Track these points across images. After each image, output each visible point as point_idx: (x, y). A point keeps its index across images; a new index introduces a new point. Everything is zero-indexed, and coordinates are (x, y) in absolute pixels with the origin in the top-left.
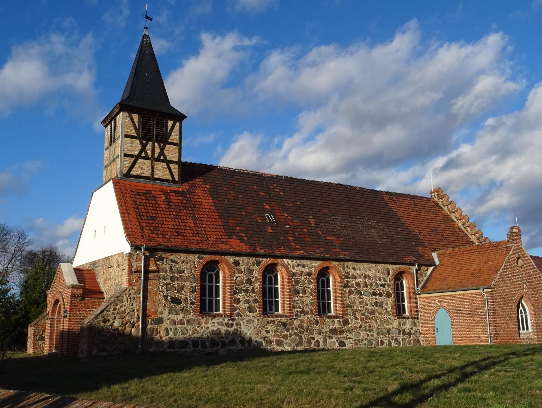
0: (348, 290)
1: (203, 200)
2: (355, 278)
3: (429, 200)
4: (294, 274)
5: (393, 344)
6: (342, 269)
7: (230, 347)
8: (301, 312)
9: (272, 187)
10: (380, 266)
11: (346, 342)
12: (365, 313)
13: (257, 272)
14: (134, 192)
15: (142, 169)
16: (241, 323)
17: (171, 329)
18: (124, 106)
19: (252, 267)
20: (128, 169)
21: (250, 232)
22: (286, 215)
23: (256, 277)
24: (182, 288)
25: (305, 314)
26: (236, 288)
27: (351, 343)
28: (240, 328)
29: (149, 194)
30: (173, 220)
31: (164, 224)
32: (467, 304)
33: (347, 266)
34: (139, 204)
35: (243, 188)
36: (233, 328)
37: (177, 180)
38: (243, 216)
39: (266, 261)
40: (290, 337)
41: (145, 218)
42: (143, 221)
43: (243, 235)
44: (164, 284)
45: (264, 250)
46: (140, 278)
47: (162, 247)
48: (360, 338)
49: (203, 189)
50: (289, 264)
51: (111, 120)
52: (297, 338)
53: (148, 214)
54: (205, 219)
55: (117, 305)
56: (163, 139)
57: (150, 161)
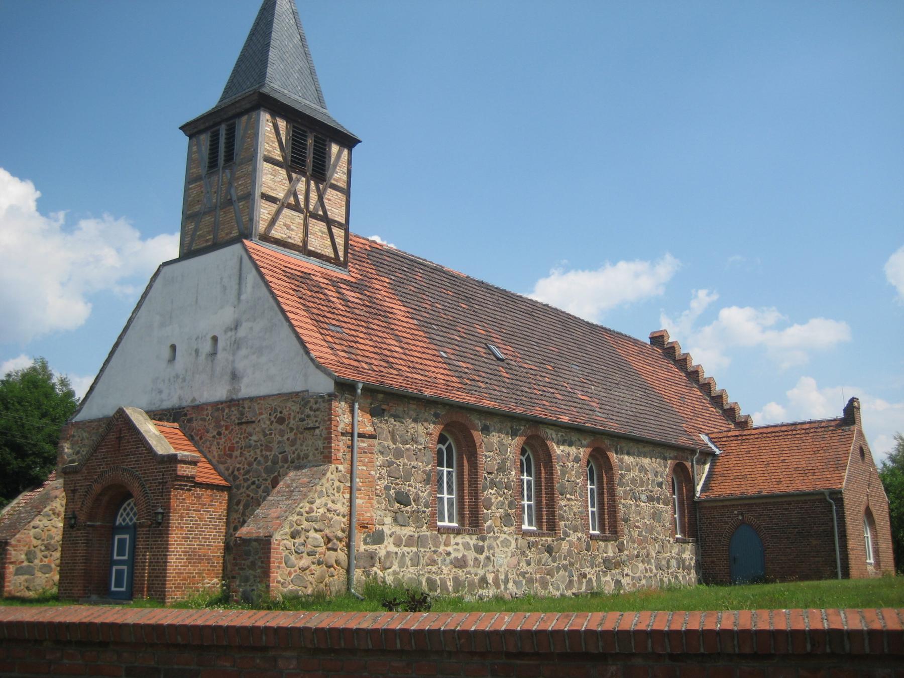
7: (480, 592)
15: (288, 227)
16: (494, 544)
17: (396, 553)
56: (320, 173)
57: (302, 216)
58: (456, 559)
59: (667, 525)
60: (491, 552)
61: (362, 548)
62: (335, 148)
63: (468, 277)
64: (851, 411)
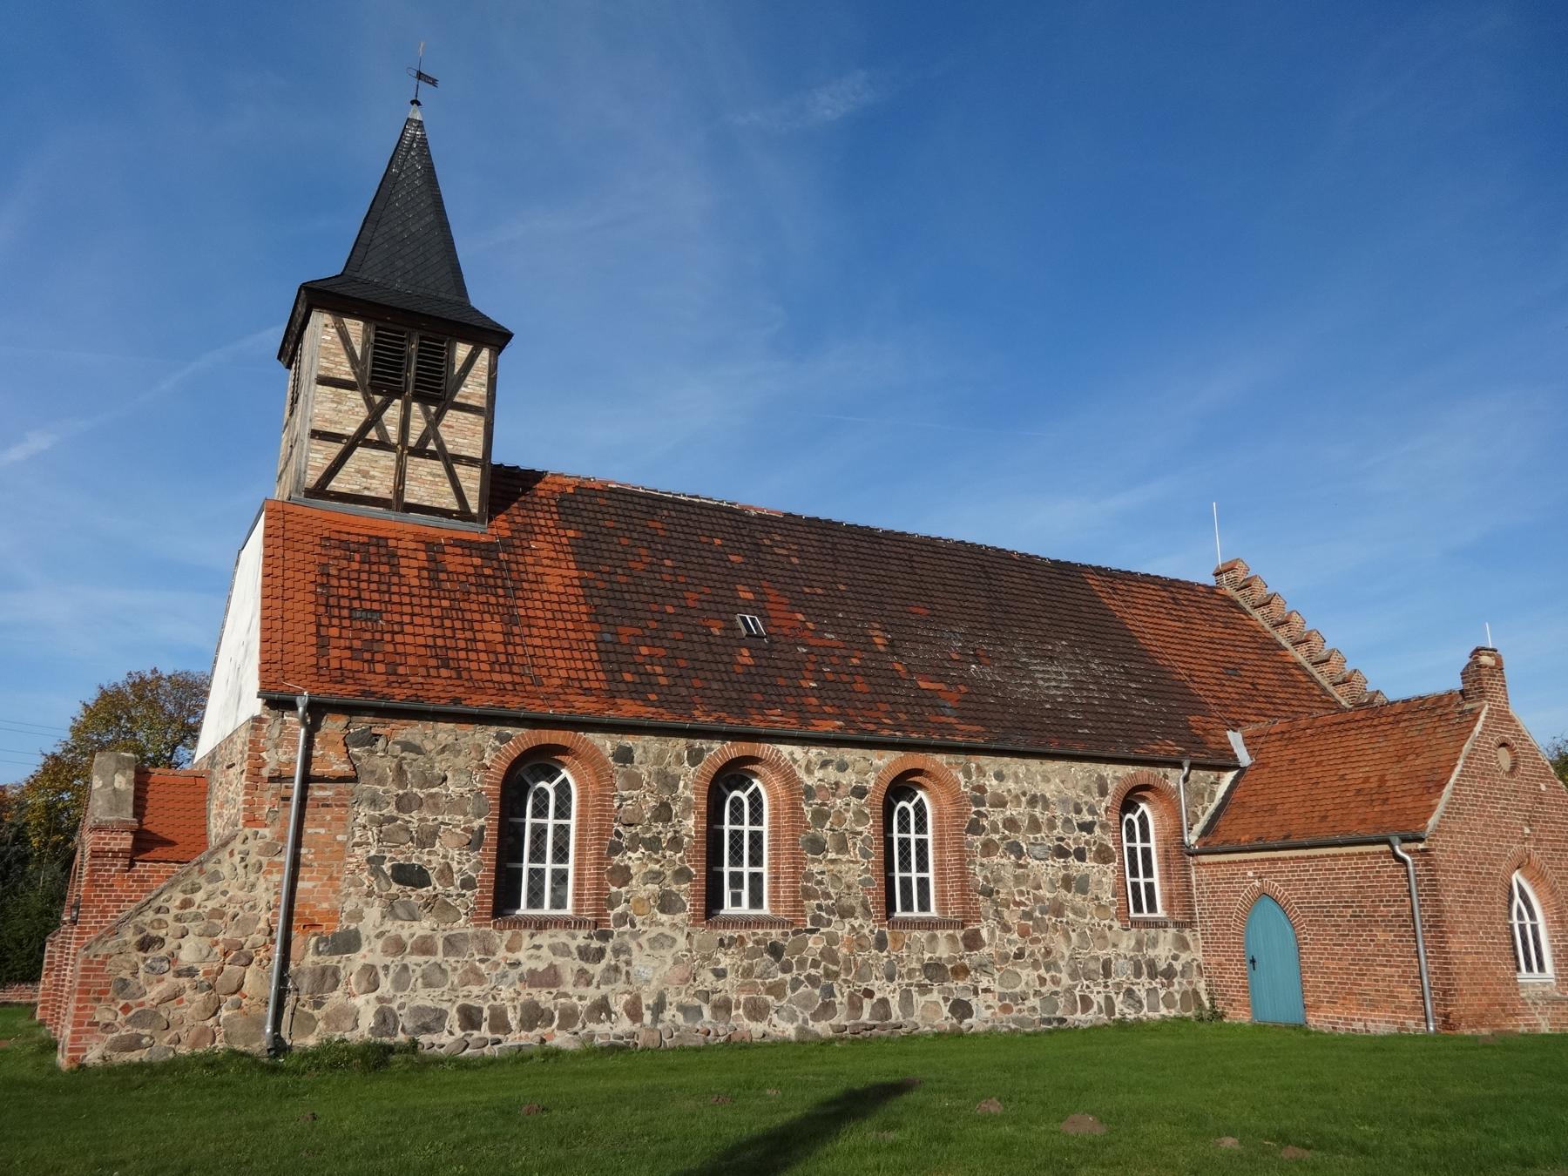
0: (978, 840)
1: (548, 570)
2: (1000, 803)
3: (1211, 590)
4: (809, 792)
5: (1119, 1005)
6: (960, 776)
7: (591, 1026)
8: (830, 911)
9: (767, 542)
10: (1078, 769)
11: (974, 1001)
12: (1033, 910)
13: (690, 785)
14: (328, 539)
15: (365, 475)
16: (633, 945)
17: (386, 968)
19: (674, 769)
20: (320, 474)
21: (682, 663)
22: (800, 617)
23: (688, 800)
24: (434, 834)
25: (842, 917)
26: (618, 834)
27: (989, 1007)
28: (628, 963)
29: (378, 546)
30: (437, 622)
31: (402, 632)
32: (1347, 887)
33: (978, 767)
34: (333, 572)
35: (679, 543)
36: (604, 963)
37: (475, 511)
38: (666, 618)
39: (722, 751)
40: (794, 990)
41: (345, 613)
42: (335, 621)
43: (659, 670)
44: (372, 820)
45: (715, 715)
46: (288, 799)
48: (1018, 990)
49: (556, 539)
50: (795, 761)
52: (817, 992)
53: (356, 604)
54: (542, 623)
55: (195, 889)
56: (437, 391)
58: (532, 972)
59: (1107, 897)
60: (623, 957)
61: (310, 959)
62: (462, 351)
64: (1481, 675)
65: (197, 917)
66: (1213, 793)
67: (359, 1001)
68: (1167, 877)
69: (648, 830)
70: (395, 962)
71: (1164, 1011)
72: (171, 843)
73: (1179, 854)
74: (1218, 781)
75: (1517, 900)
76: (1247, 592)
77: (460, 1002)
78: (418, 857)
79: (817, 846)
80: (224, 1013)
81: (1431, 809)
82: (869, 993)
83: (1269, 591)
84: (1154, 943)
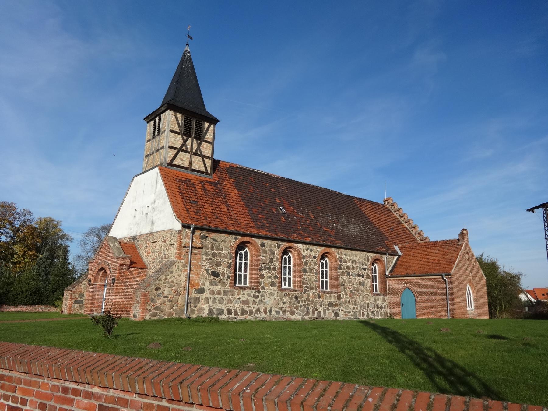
0: (340, 271)
2: (346, 262)
3: (383, 205)
4: (304, 257)
5: (370, 315)
7: (256, 315)
8: (308, 288)
10: (363, 254)
13: (277, 252)
15: (182, 160)
16: (265, 295)
17: (211, 298)
18: (169, 104)
23: (277, 257)
24: (220, 264)
32: (430, 286)
36: (259, 299)
44: (206, 259)
47: (207, 227)
51: (156, 117)
56: (200, 137)
58: (243, 301)
59: (368, 288)
62: (206, 125)
63: (281, 177)
64: (463, 235)
65: (168, 283)
66: (392, 262)
67: (204, 306)
68: (380, 283)
69: (268, 265)
70: (212, 297)
71: (380, 317)
72: (136, 263)
73: (384, 277)
74: (393, 259)
75: (467, 290)
76: (393, 207)
77: (227, 308)
78: (217, 269)
79: (305, 271)
80: (174, 308)
81: (452, 268)
82: (317, 310)
83: (398, 207)
84: (378, 300)
